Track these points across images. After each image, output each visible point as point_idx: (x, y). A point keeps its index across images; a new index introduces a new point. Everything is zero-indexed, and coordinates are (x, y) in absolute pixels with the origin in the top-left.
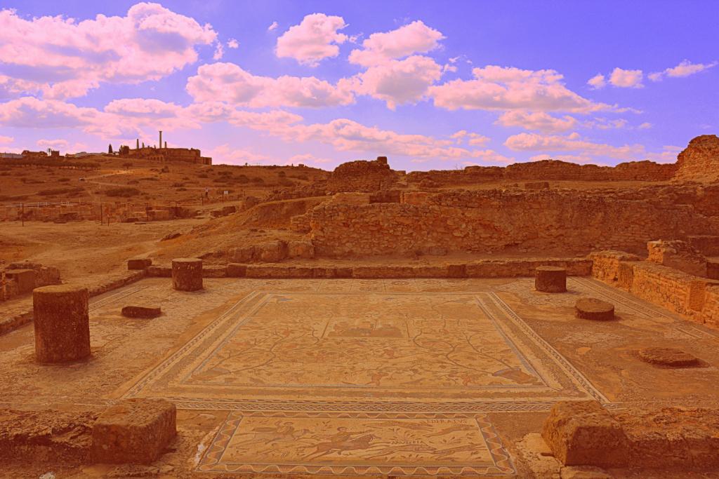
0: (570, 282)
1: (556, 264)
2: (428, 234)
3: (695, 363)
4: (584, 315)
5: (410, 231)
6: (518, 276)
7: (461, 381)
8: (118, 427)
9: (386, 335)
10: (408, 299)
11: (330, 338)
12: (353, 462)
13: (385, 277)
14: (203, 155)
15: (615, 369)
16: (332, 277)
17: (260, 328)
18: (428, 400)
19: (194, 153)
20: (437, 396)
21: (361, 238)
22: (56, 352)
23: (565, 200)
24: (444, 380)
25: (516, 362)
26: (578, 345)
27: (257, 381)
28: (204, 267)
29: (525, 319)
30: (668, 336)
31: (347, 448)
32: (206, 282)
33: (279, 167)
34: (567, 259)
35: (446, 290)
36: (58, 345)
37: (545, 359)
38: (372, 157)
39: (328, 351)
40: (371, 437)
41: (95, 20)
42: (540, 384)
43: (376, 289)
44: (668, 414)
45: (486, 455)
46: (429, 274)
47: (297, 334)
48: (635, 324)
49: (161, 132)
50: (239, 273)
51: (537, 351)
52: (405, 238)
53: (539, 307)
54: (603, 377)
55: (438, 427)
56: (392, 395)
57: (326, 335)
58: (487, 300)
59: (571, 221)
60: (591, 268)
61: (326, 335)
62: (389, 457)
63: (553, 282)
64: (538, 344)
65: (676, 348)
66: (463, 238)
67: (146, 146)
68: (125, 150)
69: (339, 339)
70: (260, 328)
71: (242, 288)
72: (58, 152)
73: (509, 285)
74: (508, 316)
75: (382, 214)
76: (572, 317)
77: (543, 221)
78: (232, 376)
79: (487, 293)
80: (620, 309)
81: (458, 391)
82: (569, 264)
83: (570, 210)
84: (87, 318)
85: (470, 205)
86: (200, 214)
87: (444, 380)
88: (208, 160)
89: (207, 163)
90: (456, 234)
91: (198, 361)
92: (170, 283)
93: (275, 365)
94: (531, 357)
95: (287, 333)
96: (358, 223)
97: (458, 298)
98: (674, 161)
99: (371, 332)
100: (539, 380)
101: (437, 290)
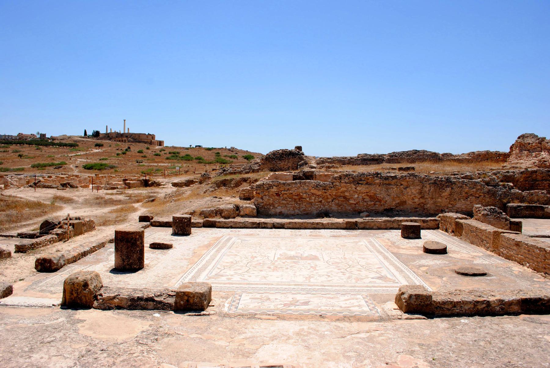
0: (423, 232)
1: (415, 221)
2: (332, 201)
3: (484, 275)
4: (427, 251)
5: (320, 199)
6: (391, 228)
7: (354, 281)
8: (188, 292)
9: (311, 259)
10: (321, 241)
11: (279, 261)
12: (302, 310)
13: (305, 228)
14: (157, 138)
15: (441, 277)
16: (271, 228)
17: (236, 255)
18: (337, 288)
19: (150, 137)
20: (341, 286)
21: (287, 204)
22: (128, 264)
23: (424, 180)
24: (345, 280)
25: (384, 273)
26: (420, 266)
27: (244, 279)
28: (192, 221)
29: (392, 253)
30: (475, 262)
31: (298, 305)
32: (193, 230)
33: (215, 149)
34: (423, 218)
35: (345, 236)
36: (129, 261)
37: (401, 271)
38: (291, 147)
39: (279, 266)
40: (309, 301)
41: (420, 238)
42: (397, 283)
43: (301, 235)
44: (458, 292)
45: (366, 309)
46: (333, 227)
47: (259, 258)
48: (458, 256)
49: (125, 120)
50: (212, 225)
51: (397, 268)
52: (317, 204)
53: (402, 247)
54: (432, 280)
55: (342, 298)
56: (317, 286)
57: (276, 259)
58: (370, 242)
59: (428, 194)
60: (439, 224)
61: (276, 259)
62: (319, 309)
63: (412, 233)
64: (398, 265)
65: (477, 268)
66: (355, 204)
67: (113, 131)
68: (96, 134)
69: (284, 261)
70: (236, 255)
71: (216, 234)
72: (44, 135)
73: (384, 234)
74: (383, 251)
75: (302, 188)
76: (421, 252)
77: (410, 193)
78: (229, 277)
79: (370, 238)
80: (450, 248)
81: (353, 285)
82: (424, 221)
83: (428, 186)
84: (143, 246)
85: (361, 182)
86: (164, 185)
87: (345, 280)
88: (160, 143)
89: (160, 145)
90: (351, 202)
91: (210, 267)
92: (170, 230)
93: (251, 272)
94: (392, 268)
95: (253, 257)
96: (286, 194)
97: (352, 241)
98: (507, 150)
99: (302, 258)
100: (397, 281)
101: (339, 236)
